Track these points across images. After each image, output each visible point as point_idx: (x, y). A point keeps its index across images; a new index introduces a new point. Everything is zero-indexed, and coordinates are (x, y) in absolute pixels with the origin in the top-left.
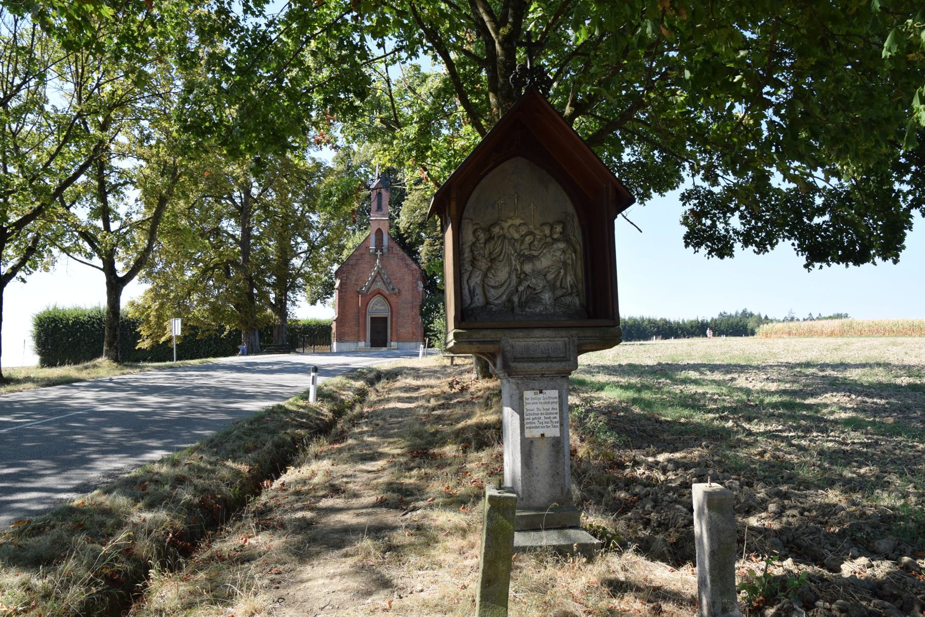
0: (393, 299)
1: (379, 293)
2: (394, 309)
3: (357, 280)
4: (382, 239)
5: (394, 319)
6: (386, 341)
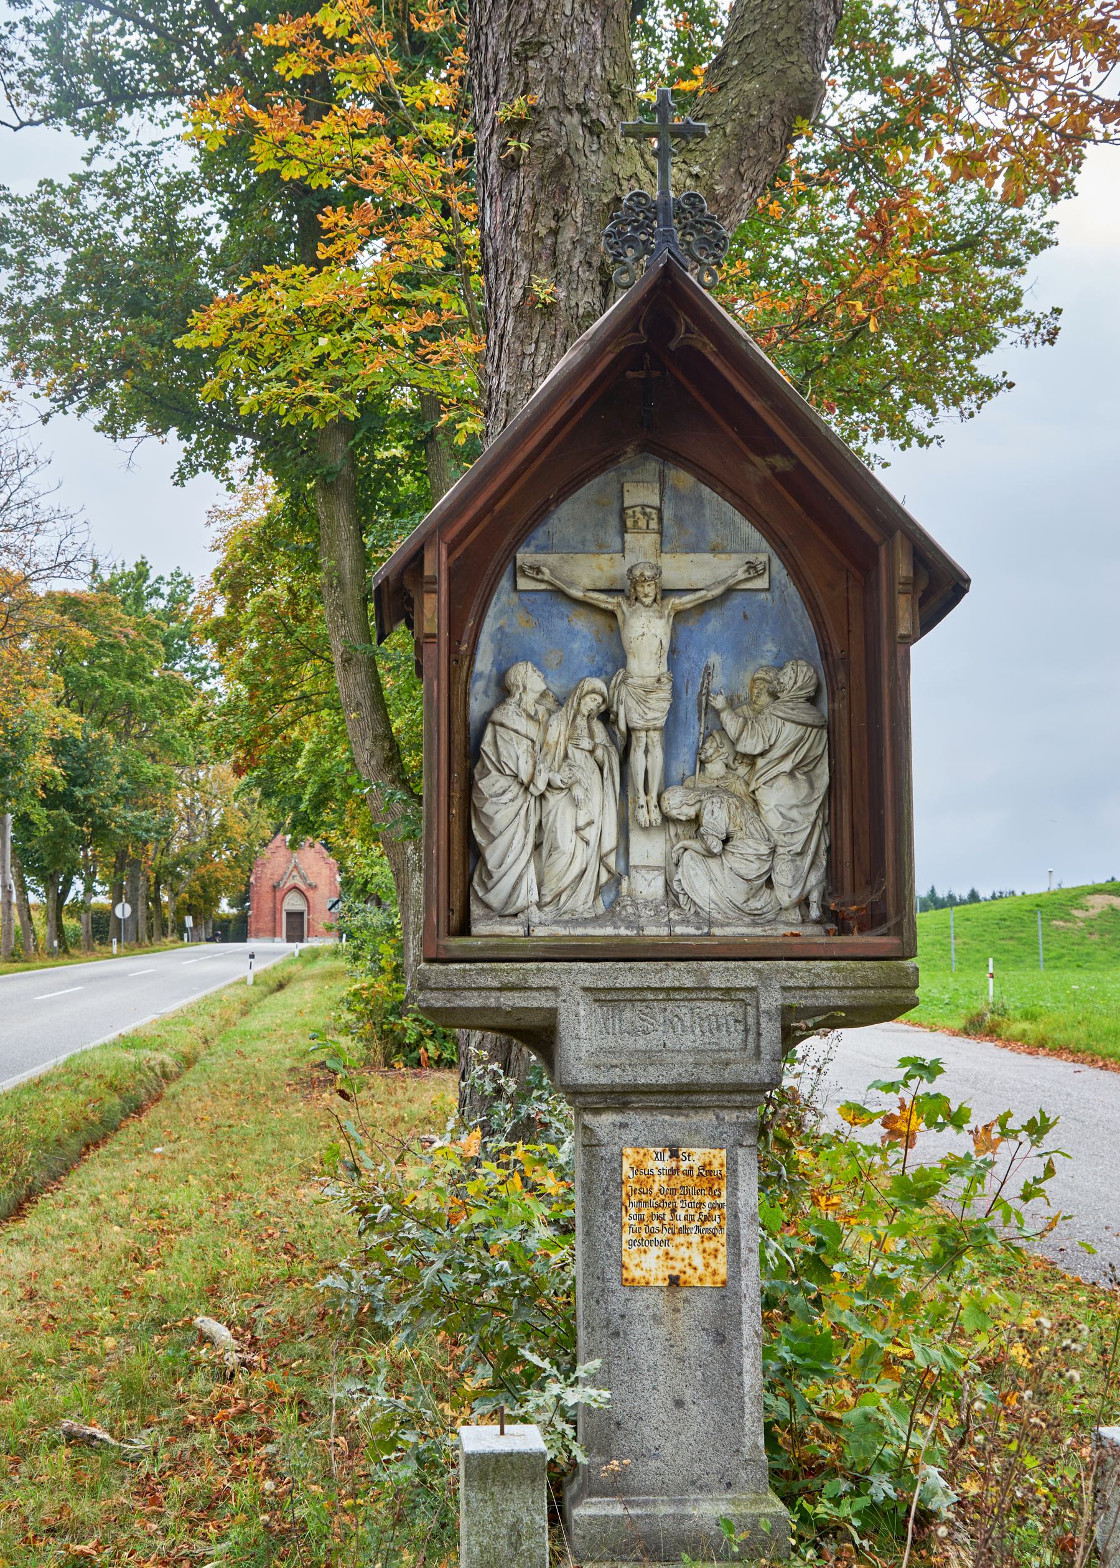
0: (309, 894)
1: (295, 888)
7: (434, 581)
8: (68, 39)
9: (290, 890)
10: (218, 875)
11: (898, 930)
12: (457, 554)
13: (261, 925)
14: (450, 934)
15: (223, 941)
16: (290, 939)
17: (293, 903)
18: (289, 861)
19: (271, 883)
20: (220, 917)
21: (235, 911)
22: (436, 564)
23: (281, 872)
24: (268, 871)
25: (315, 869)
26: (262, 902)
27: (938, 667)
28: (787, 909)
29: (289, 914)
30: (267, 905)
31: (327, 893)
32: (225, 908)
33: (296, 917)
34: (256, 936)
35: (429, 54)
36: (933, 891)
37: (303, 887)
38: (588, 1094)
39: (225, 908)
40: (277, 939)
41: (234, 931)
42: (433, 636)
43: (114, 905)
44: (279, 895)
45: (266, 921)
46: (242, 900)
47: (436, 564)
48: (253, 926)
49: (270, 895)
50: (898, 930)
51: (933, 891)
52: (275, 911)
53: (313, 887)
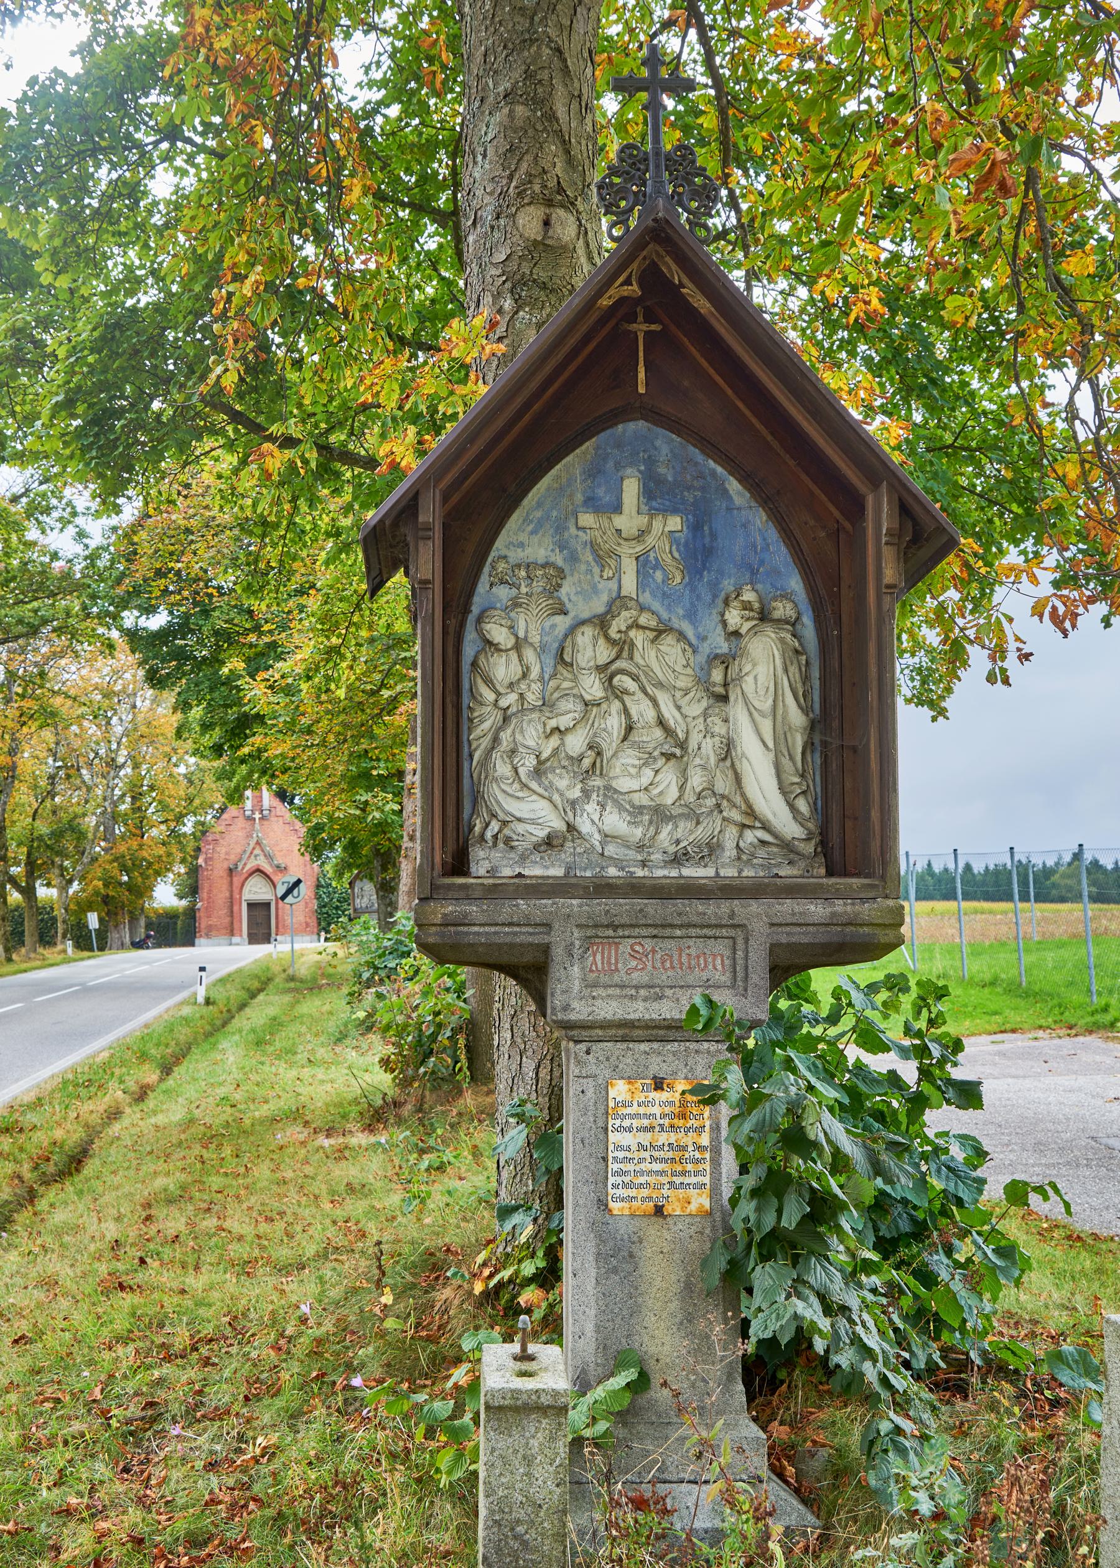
1: (258, 871)
7: (428, 528)
8: (110, 162)
10: (145, 854)
12: (455, 498)
13: (213, 921)
14: (445, 874)
15: (158, 945)
16: (253, 939)
17: (256, 890)
18: (249, 836)
19: (226, 865)
20: (156, 912)
21: (184, 903)
22: (430, 513)
23: (239, 850)
24: (222, 850)
26: (216, 888)
29: (251, 905)
30: (221, 895)
32: (165, 895)
33: (259, 909)
34: (208, 936)
37: (268, 869)
39: (165, 895)
40: (235, 939)
41: (175, 930)
42: (427, 582)
43: (367, 910)
44: (237, 881)
45: (220, 916)
46: (192, 888)
47: (430, 513)
48: (203, 922)
52: (231, 902)
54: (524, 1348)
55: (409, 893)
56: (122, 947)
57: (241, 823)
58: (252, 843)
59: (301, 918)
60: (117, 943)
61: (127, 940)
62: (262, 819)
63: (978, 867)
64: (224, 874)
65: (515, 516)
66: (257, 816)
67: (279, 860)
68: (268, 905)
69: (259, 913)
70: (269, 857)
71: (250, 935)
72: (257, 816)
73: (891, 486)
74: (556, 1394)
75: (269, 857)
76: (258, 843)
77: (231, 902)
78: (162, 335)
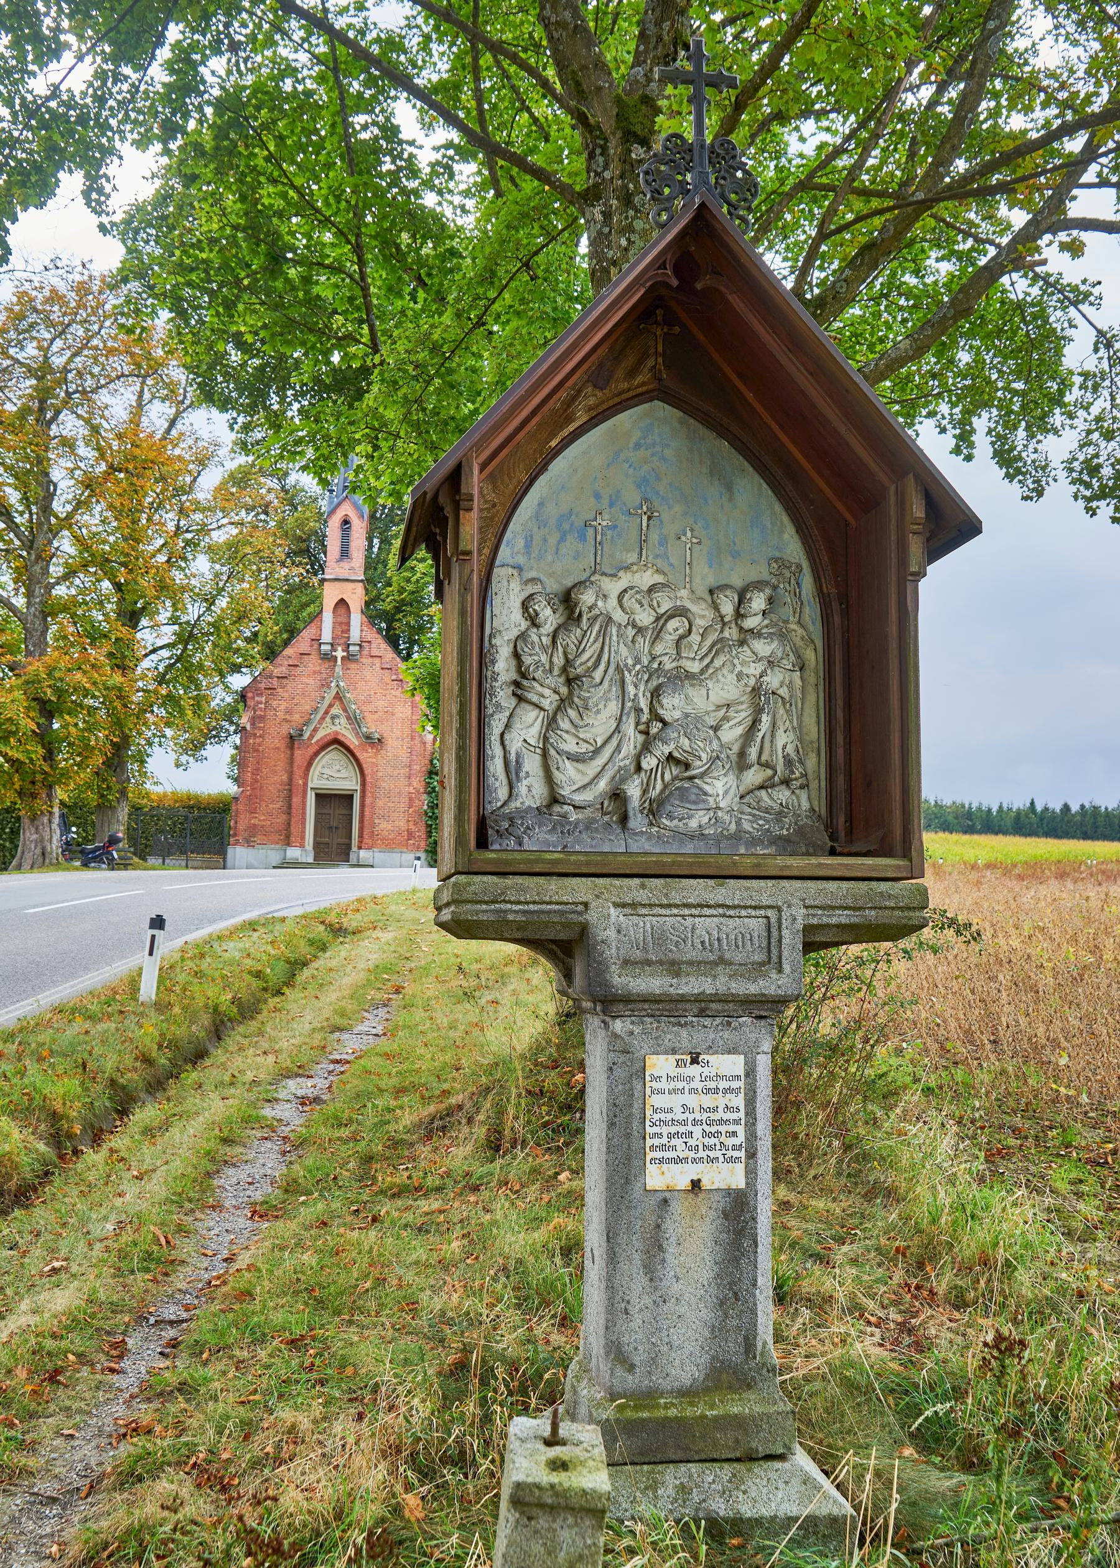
0: (366, 756)
1: (336, 742)
2: (368, 779)
3: (288, 711)
4: (348, 624)
5: (368, 801)
6: (349, 847)
9: (323, 748)
11: (906, 854)
13: (259, 819)
17: (331, 774)
19: (285, 730)
25: (381, 704)
27: (946, 596)
28: (459, 345)
29: (323, 798)
31: (404, 756)
33: (334, 803)
35: (786, 840)
36: (1032, 803)
37: (352, 740)
38: (634, 1001)
40: (293, 853)
44: (300, 755)
45: (270, 812)
49: (283, 756)
50: (906, 854)
51: (1032, 803)
52: (290, 790)
53: (375, 742)
54: (555, 1427)
55: (493, 757)
56: (43, 861)
57: (313, 663)
58: (329, 697)
59: (402, 824)
60: (34, 851)
61: (55, 845)
62: (348, 658)
63: (1075, 808)
64: (280, 743)
65: (646, 406)
66: (340, 653)
67: (371, 726)
68: (352, 796)
69: (335, 812)
70: (354, 721)
71: (317, 846)
72: (340, 653)
73: (918, 479)
74: (594, 1494)
75: (354, 721)
76: (338, 697)
77: (290, 790)
78: (994, 75)
